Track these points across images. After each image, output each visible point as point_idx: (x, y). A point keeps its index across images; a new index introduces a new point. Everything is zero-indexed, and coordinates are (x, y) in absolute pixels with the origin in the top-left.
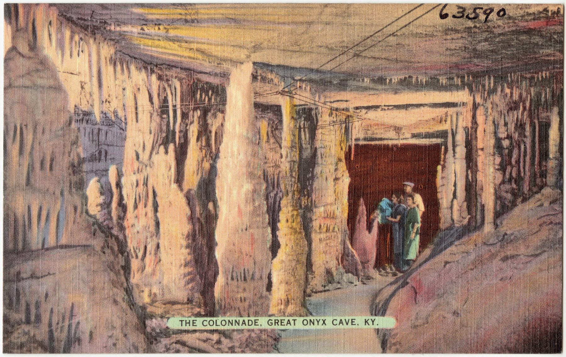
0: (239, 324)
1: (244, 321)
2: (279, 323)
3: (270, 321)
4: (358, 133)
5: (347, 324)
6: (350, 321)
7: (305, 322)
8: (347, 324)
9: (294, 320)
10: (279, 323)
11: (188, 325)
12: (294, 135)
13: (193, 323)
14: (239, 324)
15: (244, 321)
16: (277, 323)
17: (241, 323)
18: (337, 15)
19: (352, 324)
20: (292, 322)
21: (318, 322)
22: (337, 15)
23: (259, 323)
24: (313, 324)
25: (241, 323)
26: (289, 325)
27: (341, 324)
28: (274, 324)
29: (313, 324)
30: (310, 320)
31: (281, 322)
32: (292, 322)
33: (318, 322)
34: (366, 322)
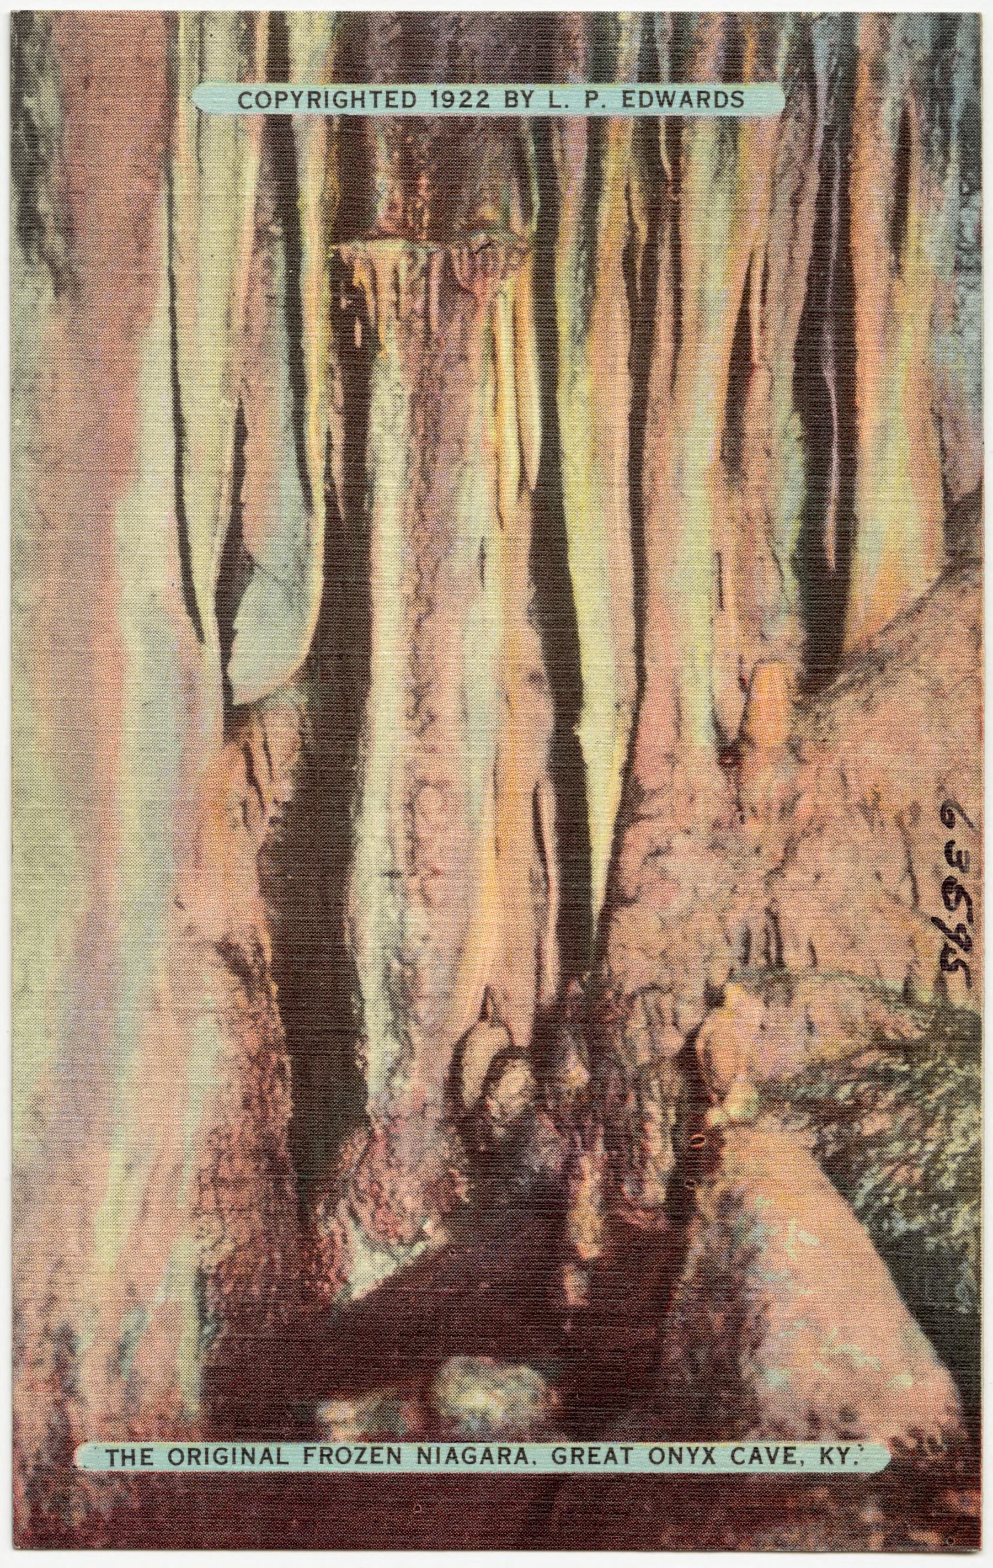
0: (252, 1460)
1: (686, 93)
2: (585, 1458)
3: (560, 1453)
4: (728, 1135)
5: (772, 1460)
6: (781, 1454)
7: (176, 1457)
8: (772, 1460)
9: (627, 1450)
10: (585, 1458)
11: (128, 1461)
12: (753, 618)
13: (143, 1456)
14: (252, 1460)
15: (686, 93)
16: (579, 1456)
17: (258, 1457)
18: (938, 209)
19: (786, 1462)
20: (620, 1455)
21: (693, 1455)
22: (938, 209)
23: (797, 1456)
24: (680, 1460)
25: (258, 1457)
26: (452, 1462)
27: (756, 1462)
28: (569, 1458)
29: (680, 1460)
30: (671, 1450)
31: (591, 1456)
32: (620, 1455)
33: (693, 1455)
34: (825, 1454)
